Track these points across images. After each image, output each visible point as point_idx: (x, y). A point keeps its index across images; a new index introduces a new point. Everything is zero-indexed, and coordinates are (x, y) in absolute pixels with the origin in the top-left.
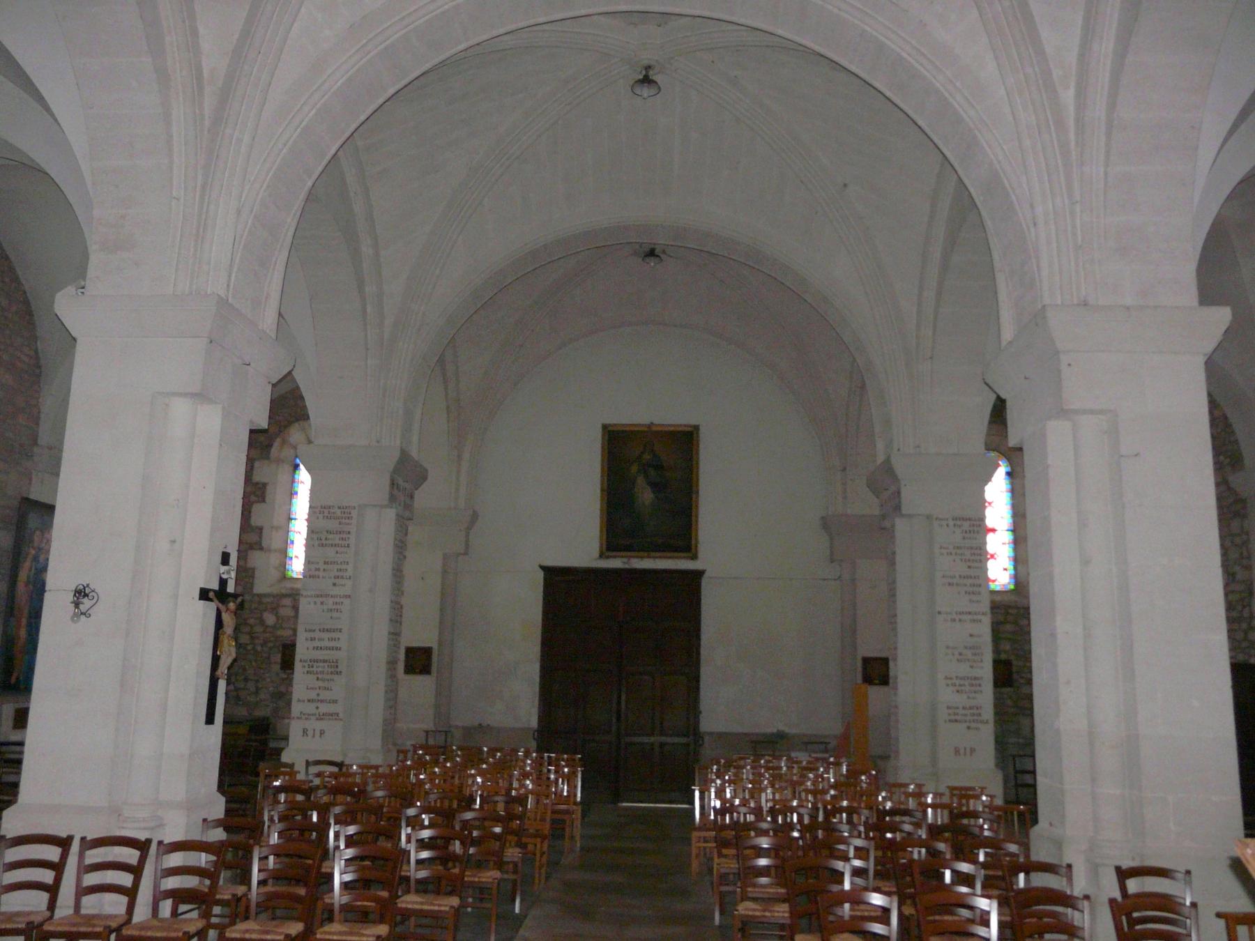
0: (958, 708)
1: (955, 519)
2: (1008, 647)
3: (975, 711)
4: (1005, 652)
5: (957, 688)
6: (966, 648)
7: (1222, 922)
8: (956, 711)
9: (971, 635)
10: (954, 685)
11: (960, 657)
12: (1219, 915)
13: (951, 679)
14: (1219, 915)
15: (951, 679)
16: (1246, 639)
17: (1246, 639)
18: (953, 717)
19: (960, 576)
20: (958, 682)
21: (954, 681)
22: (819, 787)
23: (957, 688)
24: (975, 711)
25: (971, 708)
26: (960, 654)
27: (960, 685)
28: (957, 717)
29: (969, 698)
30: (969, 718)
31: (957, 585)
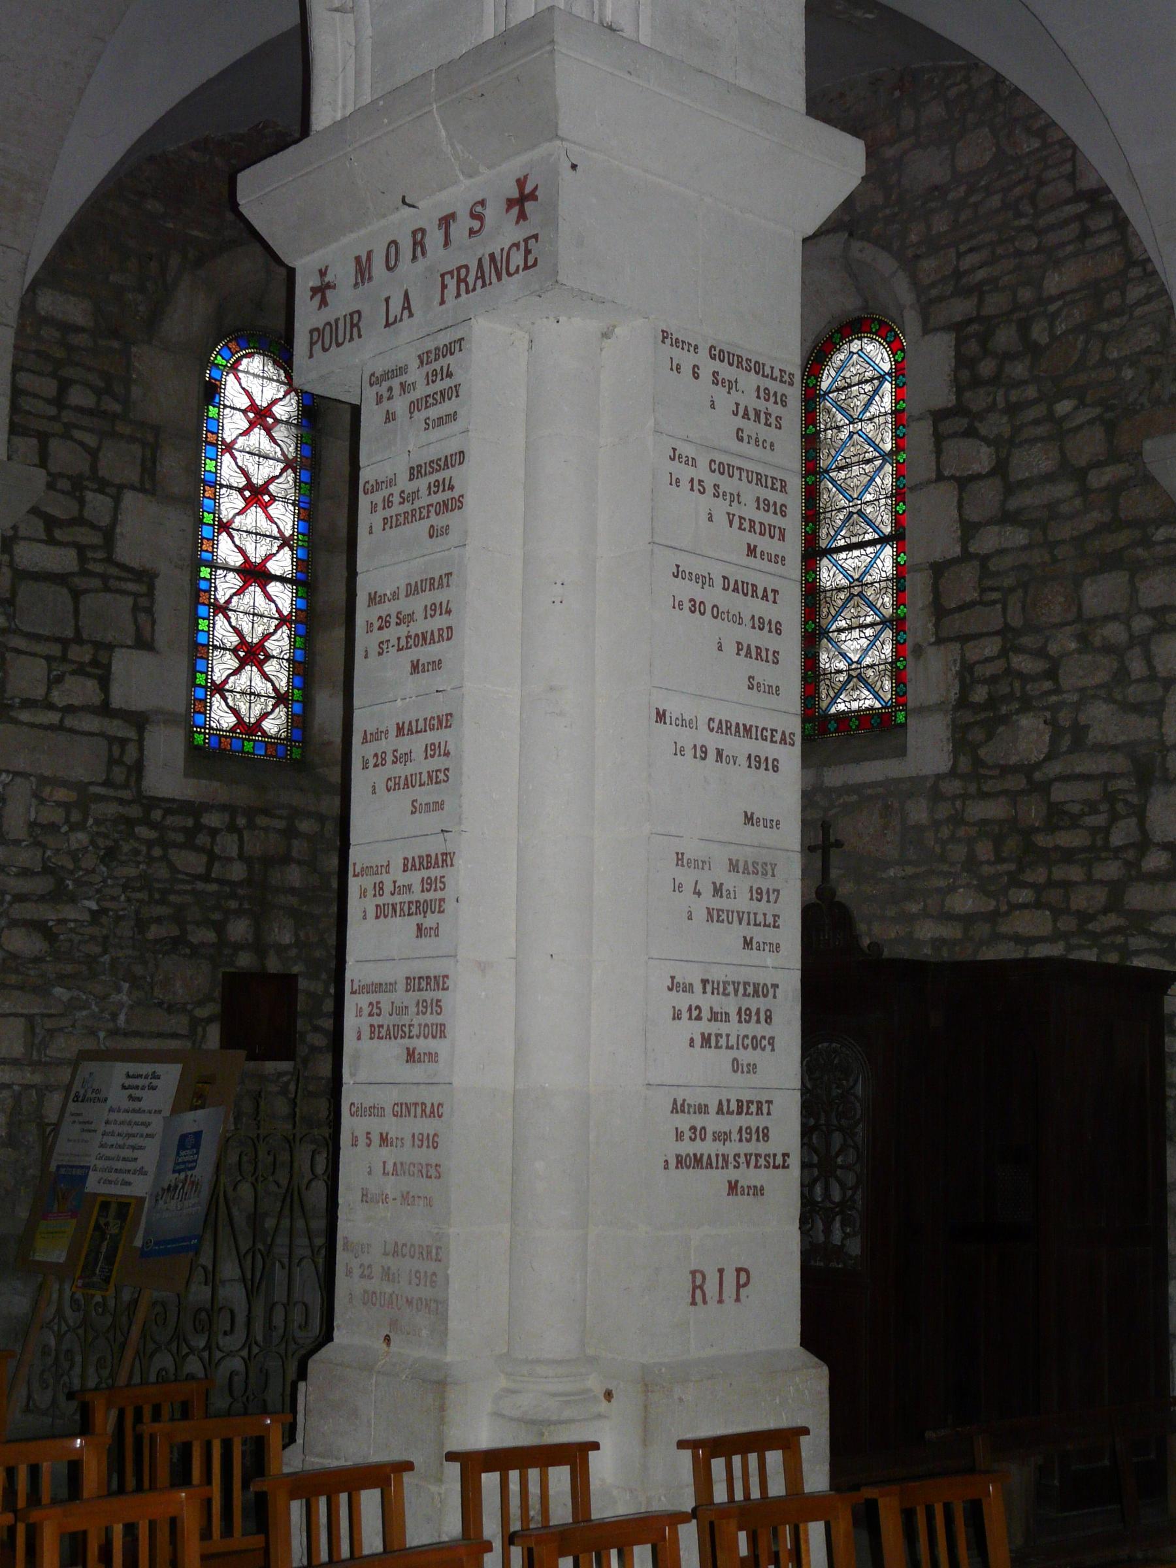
0: (703, 1109)
1: (717, 354)
2: (287, 938)
3: (753, 1121)
4: (281, 949)
5: (705, 1027)
6: (733, 866)
7: (687, 1454)
8: (699, 1121)
9: (749, 819)
10: (695, 1013)
11: (717, 903)
12: (682, 1444)
13: (688, 988)
14: (682, 1444)
15: (688, 988)
16: (1114, 904)
17: (1114, 904)
18: (688, 1148)
19: (400, 730)
20: (707, 1002)
21: (697, 998)
22: (81, 1442)
23: (705, 1027)
24: (753, 1121)
25: (742, 1108)
26: (718, 890)
27: (714, 1016)
28: (699, 1147)
29: (736, 1066)
30: (732, 1148)
31: (717, 613)
